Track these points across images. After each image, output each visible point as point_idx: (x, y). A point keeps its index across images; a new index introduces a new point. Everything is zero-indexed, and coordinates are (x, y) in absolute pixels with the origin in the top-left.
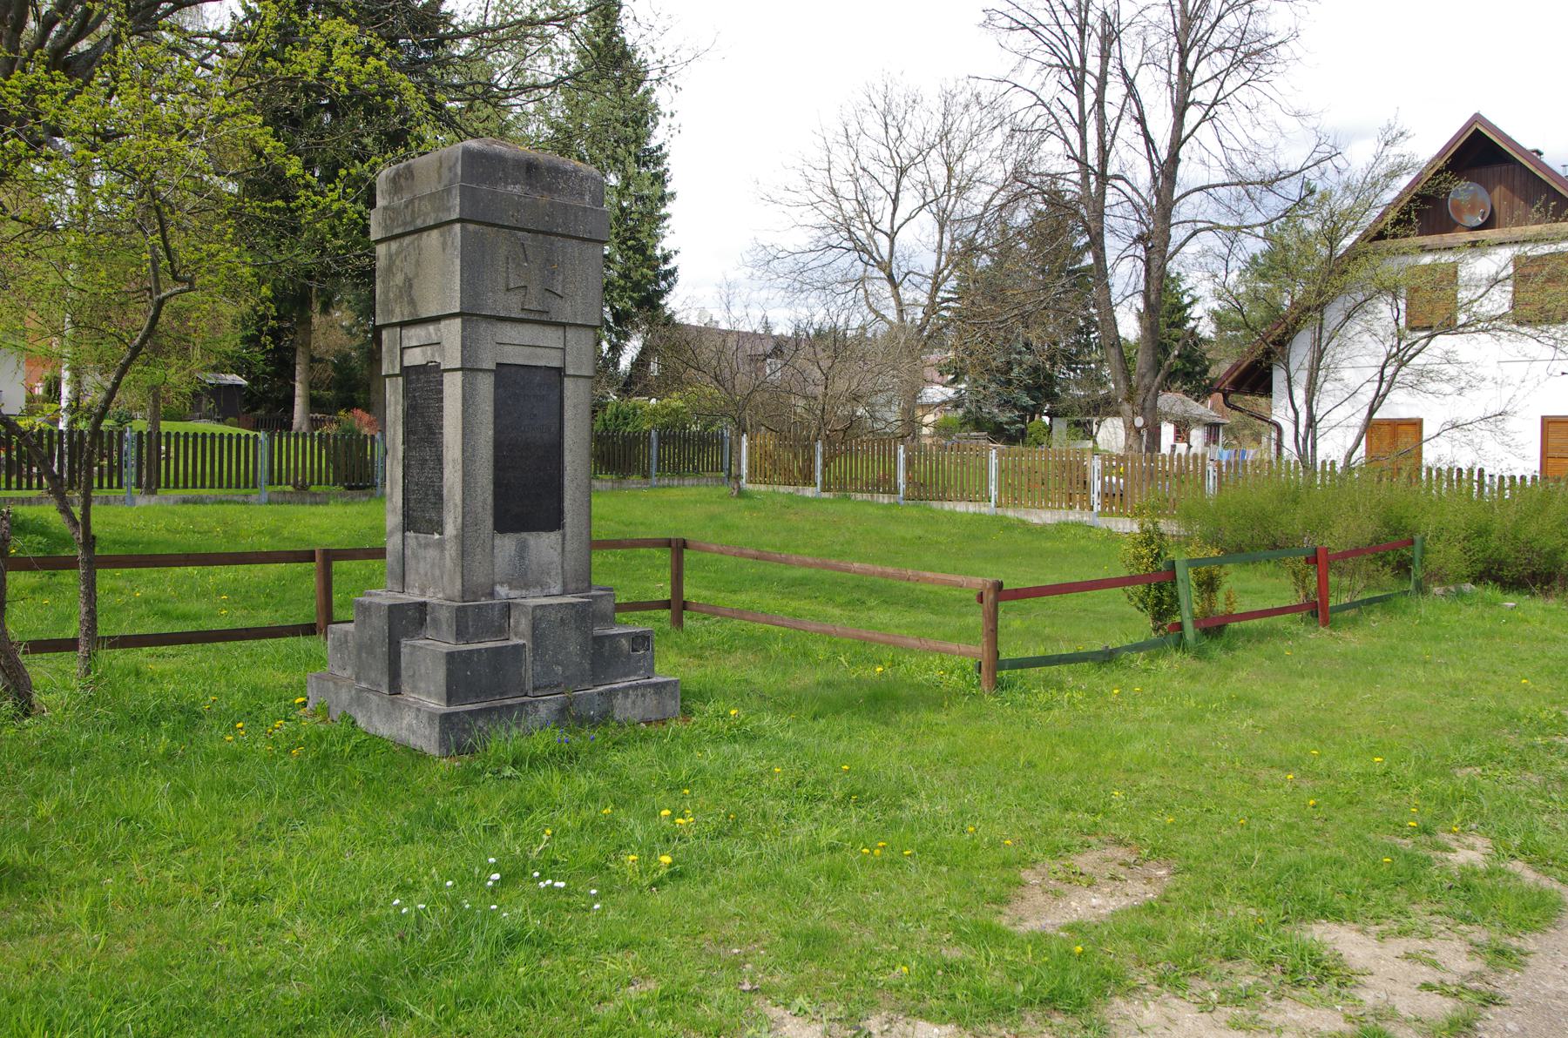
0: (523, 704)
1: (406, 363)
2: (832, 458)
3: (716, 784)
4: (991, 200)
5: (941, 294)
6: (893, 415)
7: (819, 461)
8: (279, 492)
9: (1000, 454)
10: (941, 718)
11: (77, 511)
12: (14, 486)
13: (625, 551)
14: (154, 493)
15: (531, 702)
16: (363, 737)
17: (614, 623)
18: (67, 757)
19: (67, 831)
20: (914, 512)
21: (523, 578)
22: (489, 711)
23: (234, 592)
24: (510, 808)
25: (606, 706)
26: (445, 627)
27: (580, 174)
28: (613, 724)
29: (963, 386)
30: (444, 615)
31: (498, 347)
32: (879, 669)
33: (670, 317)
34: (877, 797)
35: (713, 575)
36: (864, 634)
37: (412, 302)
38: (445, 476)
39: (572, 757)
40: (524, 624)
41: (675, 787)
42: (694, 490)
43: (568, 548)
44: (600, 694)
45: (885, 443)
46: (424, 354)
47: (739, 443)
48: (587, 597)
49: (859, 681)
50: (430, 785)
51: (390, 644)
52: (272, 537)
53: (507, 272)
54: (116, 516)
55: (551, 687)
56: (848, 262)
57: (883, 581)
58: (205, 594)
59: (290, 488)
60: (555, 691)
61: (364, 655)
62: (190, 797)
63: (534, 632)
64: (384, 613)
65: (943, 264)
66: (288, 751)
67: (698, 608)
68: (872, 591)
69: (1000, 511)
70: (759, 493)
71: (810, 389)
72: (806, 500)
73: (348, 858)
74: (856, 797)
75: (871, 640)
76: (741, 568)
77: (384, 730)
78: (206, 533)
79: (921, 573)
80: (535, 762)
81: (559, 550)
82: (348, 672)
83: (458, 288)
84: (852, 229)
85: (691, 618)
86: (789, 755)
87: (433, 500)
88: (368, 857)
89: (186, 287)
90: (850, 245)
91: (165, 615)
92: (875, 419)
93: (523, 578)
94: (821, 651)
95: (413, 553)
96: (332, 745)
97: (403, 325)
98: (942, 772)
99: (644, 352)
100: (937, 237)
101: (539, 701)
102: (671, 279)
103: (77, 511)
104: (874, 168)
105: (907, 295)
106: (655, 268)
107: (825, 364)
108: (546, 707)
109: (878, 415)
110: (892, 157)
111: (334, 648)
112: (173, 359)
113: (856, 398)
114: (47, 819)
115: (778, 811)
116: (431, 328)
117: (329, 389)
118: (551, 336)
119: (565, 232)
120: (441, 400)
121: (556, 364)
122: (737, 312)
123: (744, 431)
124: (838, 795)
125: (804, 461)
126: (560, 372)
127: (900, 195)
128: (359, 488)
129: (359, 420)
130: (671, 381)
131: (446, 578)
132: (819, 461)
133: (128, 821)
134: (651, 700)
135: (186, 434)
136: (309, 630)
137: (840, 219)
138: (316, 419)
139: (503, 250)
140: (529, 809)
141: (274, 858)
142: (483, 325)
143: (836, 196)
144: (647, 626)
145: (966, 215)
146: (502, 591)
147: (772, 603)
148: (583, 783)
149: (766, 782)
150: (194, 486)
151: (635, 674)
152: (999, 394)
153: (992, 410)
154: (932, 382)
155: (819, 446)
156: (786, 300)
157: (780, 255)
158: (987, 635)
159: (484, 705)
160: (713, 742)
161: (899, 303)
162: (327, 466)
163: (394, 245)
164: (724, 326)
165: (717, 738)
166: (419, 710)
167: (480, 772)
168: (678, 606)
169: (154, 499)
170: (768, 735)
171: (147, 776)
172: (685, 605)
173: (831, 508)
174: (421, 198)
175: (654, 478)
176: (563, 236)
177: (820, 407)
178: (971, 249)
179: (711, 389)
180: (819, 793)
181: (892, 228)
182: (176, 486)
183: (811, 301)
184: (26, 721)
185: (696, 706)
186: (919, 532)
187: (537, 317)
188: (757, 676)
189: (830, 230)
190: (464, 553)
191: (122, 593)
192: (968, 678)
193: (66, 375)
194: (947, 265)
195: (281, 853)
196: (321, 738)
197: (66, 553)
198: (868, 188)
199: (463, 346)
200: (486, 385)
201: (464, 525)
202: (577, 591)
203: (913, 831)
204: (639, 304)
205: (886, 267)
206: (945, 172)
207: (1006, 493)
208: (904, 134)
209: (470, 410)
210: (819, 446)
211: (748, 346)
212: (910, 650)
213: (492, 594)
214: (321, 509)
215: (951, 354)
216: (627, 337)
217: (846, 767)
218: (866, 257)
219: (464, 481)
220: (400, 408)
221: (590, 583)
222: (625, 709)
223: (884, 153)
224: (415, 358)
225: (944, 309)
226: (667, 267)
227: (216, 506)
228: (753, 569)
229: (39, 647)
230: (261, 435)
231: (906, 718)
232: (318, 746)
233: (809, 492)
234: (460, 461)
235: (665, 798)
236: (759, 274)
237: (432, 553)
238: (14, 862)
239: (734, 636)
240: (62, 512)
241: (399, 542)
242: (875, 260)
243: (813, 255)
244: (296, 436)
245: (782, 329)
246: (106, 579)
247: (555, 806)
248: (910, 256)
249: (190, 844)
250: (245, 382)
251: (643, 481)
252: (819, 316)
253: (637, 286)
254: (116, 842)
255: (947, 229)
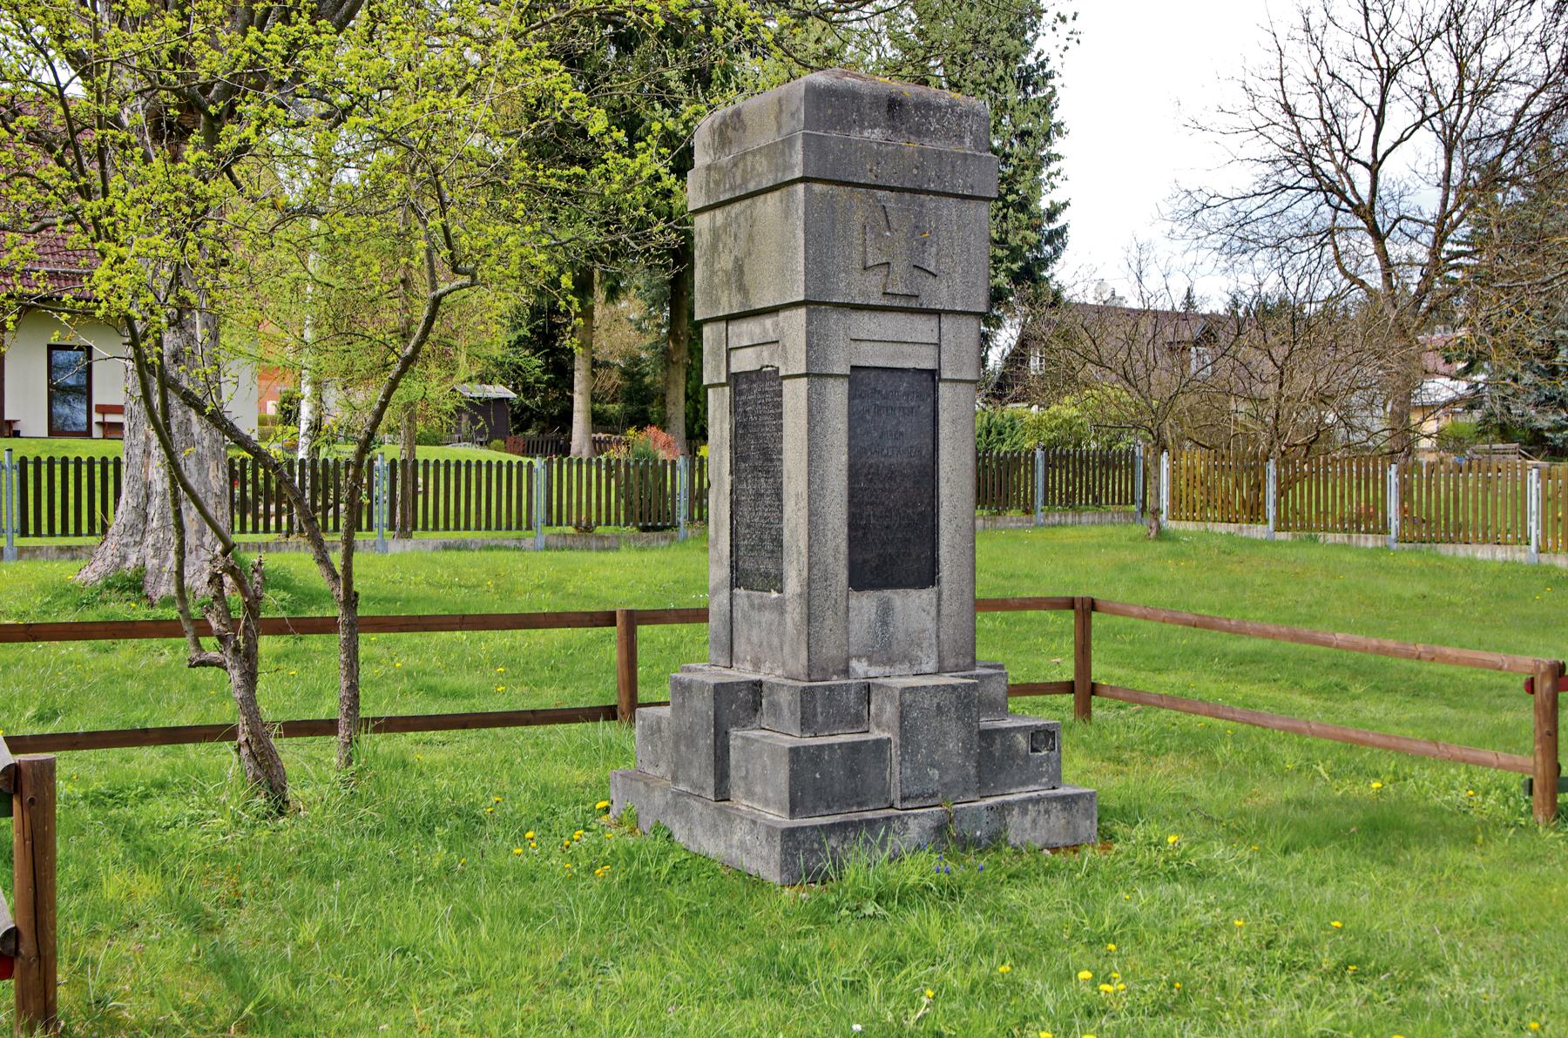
0: (888, 818)
1: (733, 369)
2: (1290, 483)
3: (1154, 940)
4: (1526, 106)
5: (1448, 246)
6: (1378, 421)
7: (1271, 489)
8: (559, 535)
9: (1545, 476)
10: (1475, 859)
11: (336, 558)
12: (249, 528)
13: (1006, 614)
14: (409, 536)
15: (898, 817)
16: (683, 856)
17: (1005, 712)
18: (328, 866)
19: (334, 962)
20: (1413, 560)
21: (885, 651)
22: (843, 826)
23: (511, 664)
24: (877, 958)
25: (996, 824)
26: (786, 712)
27: (958, 109)
28: (1008, 849)
29: (1481, 377)
30: (784, 698)
31: (853, 344)
32: (1376, 785)
33: (1057, 295)
34: (1387, 969)
35: (1128, 647)
36: (1353, 734)
37: (742, 289)
38: (786, 517)
39: (953, 893)
40: (890, 712)
41: (1095, 941)
42: (1095, 531)
43: (945, 611)
44: (990, 808)
45: (1367, 462)
46: (759, 356)
47: (1157, 464)
48: (971, 677)
49: (1342, 802)
50: (770, 922)
51: (716, 735)
52: (553, 593)
53: (864, 244)
54: (368, 566)
55: (924, 797)
56: (1309, 208)
57: (1372, 658)
58: (475, 666)
59: (571, 530)
60: (930, 802)
61: (683, 748)
62: (476, 923)
63: (901, 723)
64: (709, 694)
65: (1451, 203)
66: (590, 869)
67: (1113, 693)
68: (1356, 673)
69: (1544, 558)
70: (1185, 533)
71: (1258, 388)
72: (1254, 543)
73: (671, 1014)
74: (1352, 968)
75: (1363, 742)
76: (1168, 639)
77: (711, 846)
78: (474, 587)
79: (1438, 648)
80: (905, 897)
81: (933, 613)
82: (662, 769)
83: (801, 268)
84: (1316, 161)
85: (1101, 706)
86: (1257, 903)
87: (769, 547)
88: (697, 1013)
89: (466, 280)
90: (1312, 183)
91: (431, 691)
92: (1350, 428)
93: (885, 651)
94: (1289, 757)
95: (744, 617)
96: (644, 864)
97: (729, 318)
98: (1482, 938)
99: (1023, 342)
100: (1442, 165)
101: (909, 816)
102: (1058, 242)
103: (336, 558)
104: (1348, 73)
105: (1395, 250)
106: (1036, 228)
107: (1280, 353)
108: (918, 824)
109: (1356, 422)
110: (1374, 55)
111: (644, 738)
112: (433, 369)
113: (1323, 399)
114: (310, 945)
115: (1242, 981)
116: (768, 322)
117: (614, 401)
118: (923, 328)
119: (940, 189)
120: (780, 416)
121: (929, 364)
122: (1153, 283)
123: (1164, 448)
124: (1328, 963)
125: (1250, 488)
126: (933, 375)
127: (1387, 108)
128: (655, 529)
129: (661, 444)
130: (1063, 381)
131: (787, 649)
132: (1271, 489)
133: (404, 952)
134: (1058, 819)
135: (447, 463)
136: (610, 713)
137: (1298, 148)
138: (600, 441)
139: (858, 217)
140: (902, 961)
141: (580, 1009)
142: (834, 316)
143: (1292, 115)
144: (1042, 719)
145: (1488, 130)
146: (860, 667)
147: (1213, 688)
148: (972, 927)
149: (1222, 940)
150: (457, 528)
151: (1035, 782)
152: (1538, 388)
153: (1524, 410)
154: (1436, 373)
155: (1271, 467)
156: (1222, 265)
157: (1212, 202)
158: (1541, 740)
159: (838, 818)
160: (1144, 879)
161: (1383, 255)
162: (617, 501)
163: (719, 215)
164: (1134, 303)
165: (1149, 875)
166: (754, 822)
167: (834, 909)
168: (1084, 689)
169: (409, 544)
170: (1221, 872)
171: (423, 895)
172: (1094, 689)
173: (1291, 554)
174: (753, 153)
175: (1040, 514)
176: (936, 193)
177: (1272, 412)
178: (1493, 177)
179: (1114, 390)
180: (1300, 959)
181: (1375, 155)
182: (436, 528)
183: (1259, 265)
184: (281, 821)
185: (1119, 828)
186: (1422, 587)
187: (903, 303)
188: (1199, 789)
189: (1283, 164)
190: (810, 618)
191: (379, 663)
192: (1512, 802)
193: (307, 390)
194: (1456, 207)
195: (589, 1003)
196: (631, 856)
197: (313, 613)
198: (1338, 103)
199: (809, 344)
200: (837, 395)
201: (810, 582)
202: (957, 668)
203: (1444, 1022)
204: (1016, 278)
205: (1365, 211)
206: (1454, 70)
207: (1555, 530)
208: (1393, 21)
209: (818, 429)
210: (1271, 467)
211: (1169, 331)
212: (1420, 757)
213: (846, 672)
214: (611, 556)
215: (1462, 332)
216: (998, 323)
217: (1337, 924)
218: (1335, 199)
219: (810, 521)
220: (727, 426)
221: (974, 658)
222: (1020, 829)
223: (1364, 50)
224: (744, 362)
225: (1456, 267)
226: (1053, 226)
227: (484, 554)
228: (1186, 639)
229: (294, 729)
230: (538, 462)
231: (1419, 856)
232: (628, 865)
233: (1258, 531)
234: (805, 496)
235: (1082, 956)
236: (1180, 230)
237: (768, 616)
238: (276, 997)
239: (1163, 732)
240: (319, 562)
241: (726, 601)
242: (1350, 203)
243: (1259, 200)
244: (580, 462)
245: (1214, 302)
246: (369, 643)
247: (933, 959)
248: (1401, 195)
249: (479, 985)
250: (512, 395)
251: (1025, 517)
252: (1271, 285)
253: (1015, 254)
254: (391, 979)
255: (1456, 154)
